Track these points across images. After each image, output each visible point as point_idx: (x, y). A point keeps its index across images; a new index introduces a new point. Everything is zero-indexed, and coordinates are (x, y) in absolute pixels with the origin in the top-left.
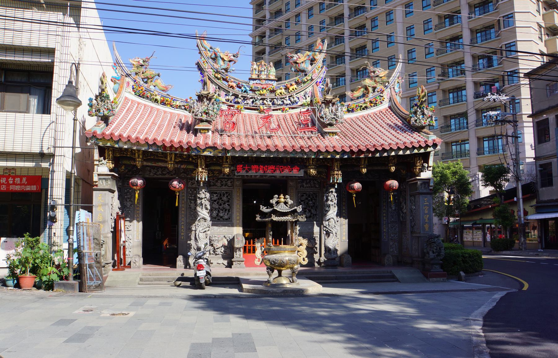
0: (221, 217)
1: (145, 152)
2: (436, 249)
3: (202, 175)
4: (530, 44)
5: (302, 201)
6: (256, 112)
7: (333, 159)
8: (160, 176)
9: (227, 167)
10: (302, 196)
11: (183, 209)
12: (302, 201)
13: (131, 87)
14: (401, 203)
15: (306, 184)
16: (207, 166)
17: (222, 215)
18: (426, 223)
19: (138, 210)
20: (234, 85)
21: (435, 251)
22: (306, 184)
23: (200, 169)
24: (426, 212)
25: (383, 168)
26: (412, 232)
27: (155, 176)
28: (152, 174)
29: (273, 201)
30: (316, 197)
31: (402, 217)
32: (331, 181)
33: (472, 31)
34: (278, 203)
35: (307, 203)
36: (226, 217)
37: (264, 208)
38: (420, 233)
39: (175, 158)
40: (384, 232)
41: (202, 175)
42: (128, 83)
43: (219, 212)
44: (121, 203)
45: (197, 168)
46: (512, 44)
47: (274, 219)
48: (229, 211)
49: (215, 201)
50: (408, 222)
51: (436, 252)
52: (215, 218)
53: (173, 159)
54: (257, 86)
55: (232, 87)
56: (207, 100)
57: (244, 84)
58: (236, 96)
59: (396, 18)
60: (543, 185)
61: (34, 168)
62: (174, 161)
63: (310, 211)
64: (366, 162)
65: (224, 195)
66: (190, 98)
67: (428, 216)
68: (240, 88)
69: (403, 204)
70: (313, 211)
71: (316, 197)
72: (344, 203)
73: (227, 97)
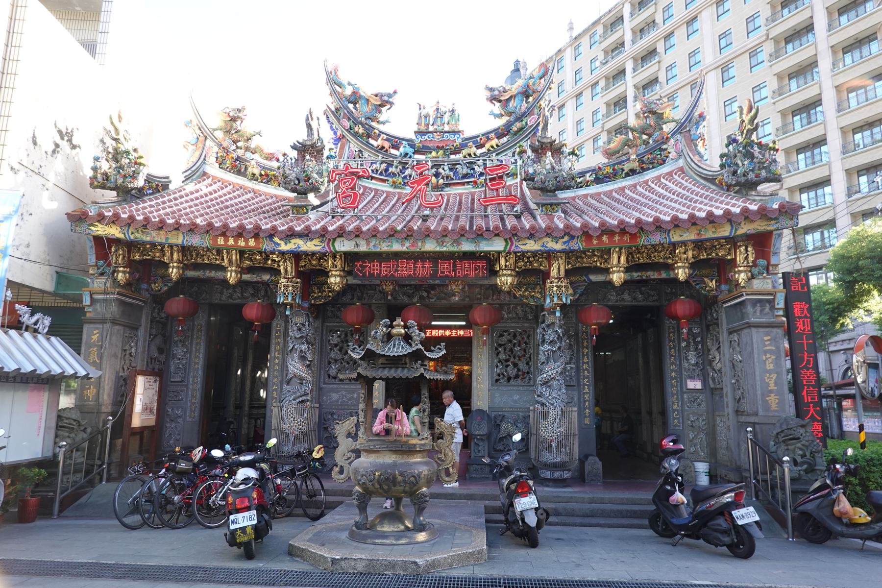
2: (803, 456)
4: (793, 586)
5: (500, 345)
9: (335, 276)
10: (501, 336)
11: (277, 361)
12: (500, 345)
15: (509, 313)
18: (771, 392)
20: (387, 145)
21: (799, 459)
22: (509, 313)
24: (770, 366)
25: (664, 275)
26: (737, 412)
28: (224, 298)
30: (528, 337)
31: (713, 379)
33: (848, 172)
34: (389, 337)
35: (511, 350)
38: (756, 414)
40: (674, 410)
49: (336, 345)
50: (727, 390)
51: (803, 463)
52: (335, 378)
59: (704, 58)
63: (515, 365)
66: (284, 155)
67: (774, 376)
69: (714, 352)
70: (522, 366)
71: (528, 337)
72: (585, 351)
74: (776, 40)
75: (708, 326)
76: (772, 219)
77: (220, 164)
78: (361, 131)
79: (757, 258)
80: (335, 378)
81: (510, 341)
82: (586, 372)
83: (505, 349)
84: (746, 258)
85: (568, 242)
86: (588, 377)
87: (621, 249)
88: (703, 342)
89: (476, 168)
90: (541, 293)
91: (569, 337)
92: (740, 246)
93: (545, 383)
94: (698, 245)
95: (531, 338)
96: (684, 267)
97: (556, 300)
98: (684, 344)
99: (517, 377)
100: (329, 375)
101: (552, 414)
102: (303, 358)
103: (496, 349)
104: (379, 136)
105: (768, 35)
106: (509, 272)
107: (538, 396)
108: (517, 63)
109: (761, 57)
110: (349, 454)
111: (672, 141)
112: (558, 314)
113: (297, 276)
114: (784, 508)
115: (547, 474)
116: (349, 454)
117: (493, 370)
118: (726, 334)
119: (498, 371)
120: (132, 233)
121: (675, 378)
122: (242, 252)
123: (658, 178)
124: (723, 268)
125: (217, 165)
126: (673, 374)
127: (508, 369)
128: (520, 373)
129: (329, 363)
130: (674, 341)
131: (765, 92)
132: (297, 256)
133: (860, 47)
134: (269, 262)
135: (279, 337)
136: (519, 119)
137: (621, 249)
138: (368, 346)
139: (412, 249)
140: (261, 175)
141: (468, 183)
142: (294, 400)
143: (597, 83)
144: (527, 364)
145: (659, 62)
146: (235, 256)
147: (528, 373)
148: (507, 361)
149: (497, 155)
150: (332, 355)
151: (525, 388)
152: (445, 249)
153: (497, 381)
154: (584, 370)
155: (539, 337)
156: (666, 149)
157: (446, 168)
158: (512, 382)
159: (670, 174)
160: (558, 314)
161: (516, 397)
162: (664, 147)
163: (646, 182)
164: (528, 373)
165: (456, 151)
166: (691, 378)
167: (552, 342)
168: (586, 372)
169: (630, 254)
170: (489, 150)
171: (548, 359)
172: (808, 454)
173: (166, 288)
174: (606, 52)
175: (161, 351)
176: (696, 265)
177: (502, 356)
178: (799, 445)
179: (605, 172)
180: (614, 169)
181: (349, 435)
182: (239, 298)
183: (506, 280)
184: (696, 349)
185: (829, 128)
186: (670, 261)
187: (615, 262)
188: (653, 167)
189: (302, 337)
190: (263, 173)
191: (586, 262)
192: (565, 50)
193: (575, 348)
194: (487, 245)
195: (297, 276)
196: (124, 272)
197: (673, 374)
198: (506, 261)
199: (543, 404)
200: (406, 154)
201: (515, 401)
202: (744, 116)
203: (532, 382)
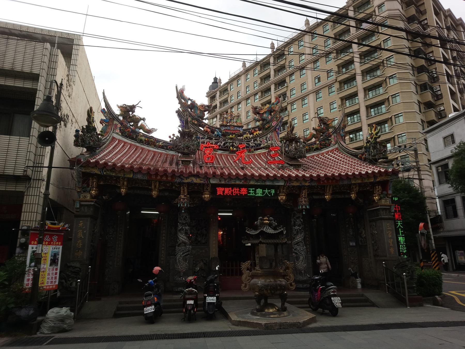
6: (227, 152)
9: (207, 194)
11: (164, 235)
13: (118, 128)
18: (391, 247)
20: (209, 130)
23: (182, 196)
24: (390, 236)
29: (258, 223)
38: (386, 256)
44: (181, 120)
45: (27, 293)
46: (400, 115)
55: (207, 131)
56: (188, 137)
59: (308, 87)
60: (448, 217)
64: (331, 191)
66: (174, 135)
67: (392, 240)
74: (340, 82)
76: (389, 175)
78: (196, 122)
79: (383, 191)
82: (307, 239)
87: (330, 186)
93: (297, 244)
97: (304, 207)
98: (347, 226)
101: (301, 258)
105: (336, 80)
106: (284, 194)
107: (295, 250)
108: (215, 79)
109: (334, 89)
110: (249, 278)
111: (333, 136)
113: (188, 194)
114: (405, 295)
116: (249, 278)
120: (105, 171)
122: (160, 182)
123: (328, 152)
126: (344, 239)
131: (335, 106)
133: (375, 89)
136: (268, 123)
137: (330, 186)
139: (245, 183)
140: (145, 140)
142: (183, 254)
143: (257, 93)
145: (287, 87)
159: (332, 150)
162: (330, 138)
163: (323, 153)
165: (241, 135)
167: (299, 226)
168: (307, 239)
171: (297, 232)
173: (111, 198)
174: (261, 79)
178: (407, 268)
181: (248, 269)
185: (363, 124)
189: (186, 223)
192: (241, 76)
194: (277, 183)
195: (188, 194)
196: (95, 190)
199: (296, 253)
200: (218, 135)
202: (373, 132)
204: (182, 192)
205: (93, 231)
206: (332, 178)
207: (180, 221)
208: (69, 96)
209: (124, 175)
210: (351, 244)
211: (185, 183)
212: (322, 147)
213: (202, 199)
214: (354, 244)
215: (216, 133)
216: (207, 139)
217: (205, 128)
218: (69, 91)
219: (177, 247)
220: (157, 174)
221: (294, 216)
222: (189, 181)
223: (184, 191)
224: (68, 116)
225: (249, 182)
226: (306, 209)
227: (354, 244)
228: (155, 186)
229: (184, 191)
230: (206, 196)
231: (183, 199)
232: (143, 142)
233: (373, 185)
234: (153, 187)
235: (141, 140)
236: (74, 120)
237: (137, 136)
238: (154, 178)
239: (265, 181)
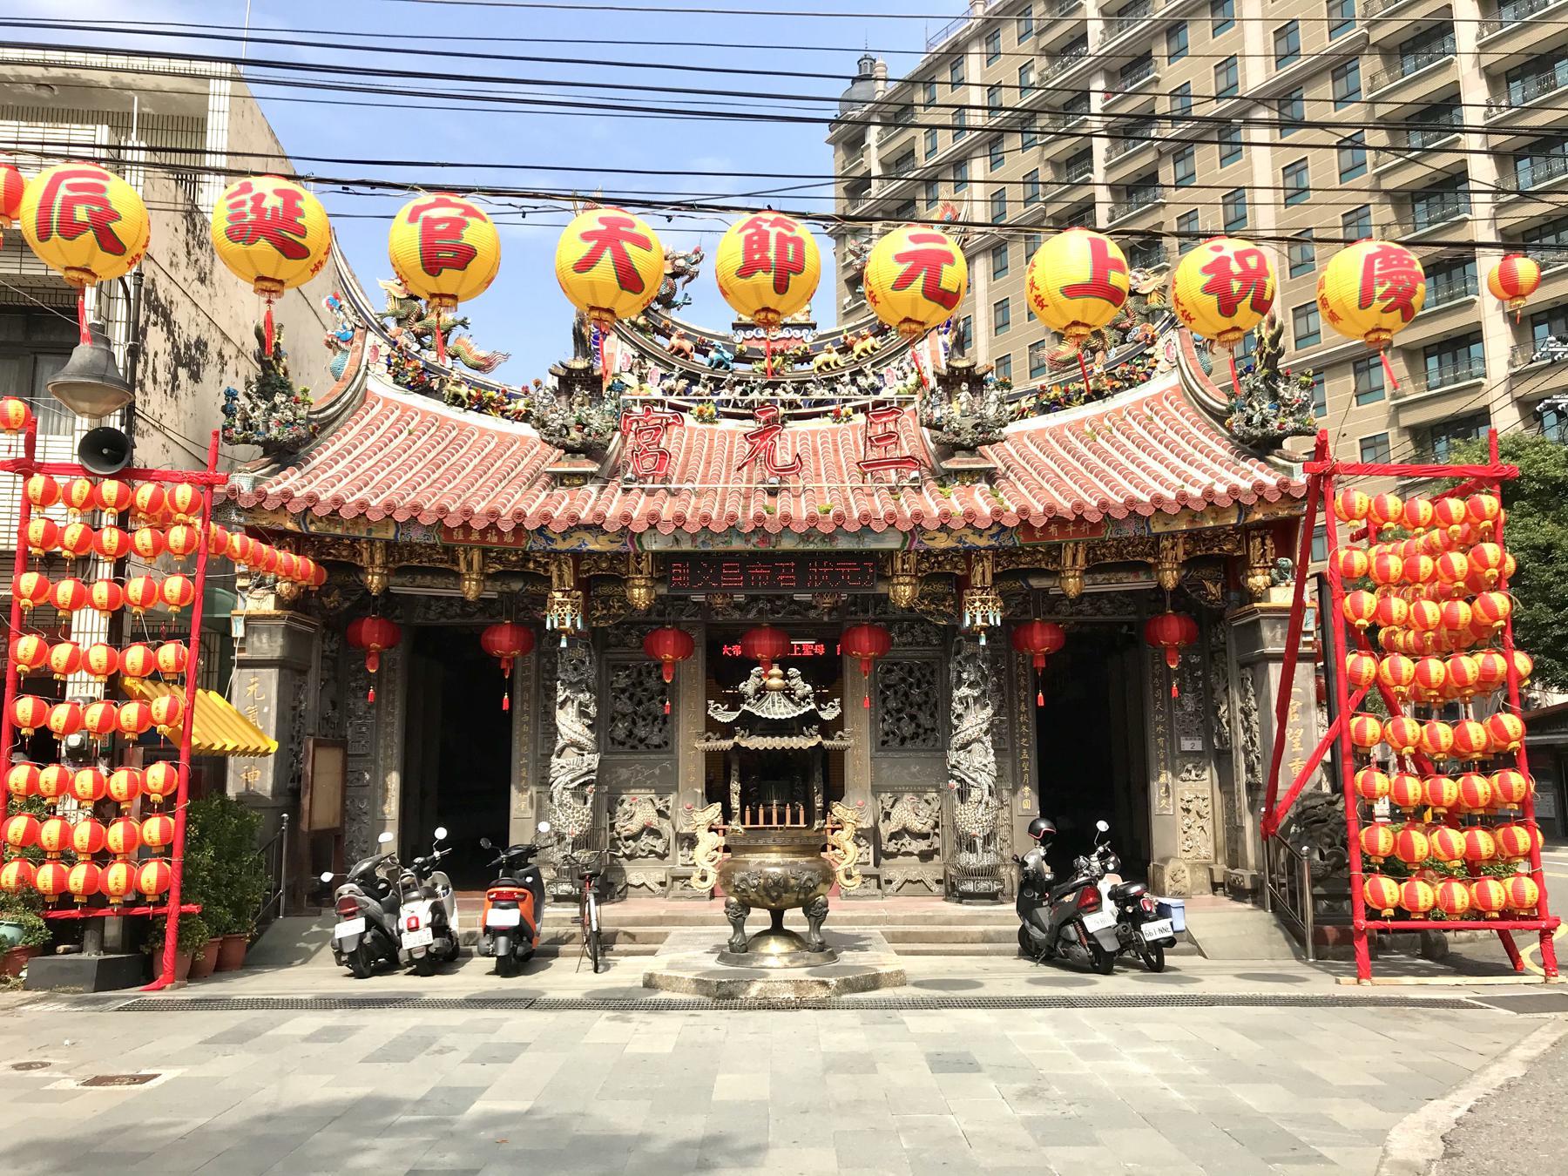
0: (641, 741)
1: (389, 546)
3: (562, 614)
5: (888, 687)
7: (969, 555)
8: (457, 620)
9: (639, 587)
10: (889, 671)
11: (526, 718)
12: (888, 687)
13: (384, 360)
14: (1213, 691)
15: (901, 634)
16: (580, 584)
17: (643, 734)
19: (387, 725)
20: (687, 345)
22: (901, 634)
23: (558, 596)
27: (443, 620)
28: (431, 615)
29: (748, 687)
32: (968, 622)
34: (762, 692)
35: (906, 694)
36: (656, 740)
37: (721, 709)
39: (484, 565)
41: (562, 614)
42: (375, 349)
43: (634, 723)
47: (743, 744)
48: (665, 722)
49: (623, 691)
52: (623, 744)
53: (476, 566)
54: (754, 345)
55: (680, 351)
57: (716, 342)
58: (693, 379)
61: (1003, 697)
62: (481, 572)
63: (913, 718)
65: (649, 673)
66: (537, 384)
68: (706, 354)
70: (924, 719)
71: (932, 673)
72: (1023, 694)
73: (668, 383)
75: (1212, 653)
77: (395, 377)
80: (623, 744)
81: (903, 680)
83: (896, 693)
84: (1263, 555)
85: (998, 534)
86: (1027, 735)
87: (1076, 544)
88: (1205, 678)
89: (839, 387)
90: (954, 606)
91: (998, 673)
92: (1254, 537)
94: (1194, 536)
95: (937, 675)
96: (1172, 570)
99: (915, 736)
100: (613, 739)
102: (583, 714)
103: (882, 692)
104: (673, 329)
106: (907, 579)
112: (983, 642)
115: (969, 887)
117: (877, 725)
118: (1235, 666)
119: (886, 728)
121: (1163, 735)
122: (485, 552)
124: (1233, 570)
125: (390, 378)
127: (902, 724)
128: (921, 731)
129: (613, 719)
130: (1160, 677)
132: (578, 556)
134: (531, 565)
135: (527, 678)
137: (1076, 544)
138: (745, 707)
141: (825, 414)
144: (932, 715)
146: (476, 556)
147: (933, 730)
148: (899, 711)
149: (873, 365)
150: (619, 706)
151: (928, 755)
152: (811, 547)
153: (884, 743)
154: (1021, 724)
155: (953, 675)
156: (1151, 356)
157: (789, 389)
158: (908, 745)
160: (983, 642)
161: (914, 769)
164: (933, 730)
165: (806, 358)
166: (1187, 734)
167: (971, 685)
169: (1090, 549)
170: (859, 356)
172: (1338, 842)
173: (347, 605)
175: (334, 705)
176: (1190, 563)
177: (892, 704)
178: (1326, 830)
179: (1052, 395)
180: (1067, 391)
182: (457, 615)
183: (904, 592)
184: (1195, 690)
186: (1151, 560)
187: (1069, 563)
188: (1131, 386)
189: (580, 681)
190: (473, 393)
191: (1025, 563)
193: (1006, 689)
197: (1160, 728)
198: (904, 562)
200: (720, 364)
201: (914, 775)
203: (939, 745)
204: (555, 580)
205: (294, 708)
206: (1073, 517)
207: (562, 676)
208: (202, 281)
209: (370, 531)
210: (1187, 745)
211: (561, 552)
212: (1118, 384)
213: (627, 604)
214: (1198, 746)
215: (713, 354)
216: (681, 377)
217: (674, 340)
218: (201, 262)
219: (554, 758)
220: (466, 527)
221: (958, 653)
222: (571, 544)
223: (560, 577)
224: (201, 345)
225: (778, 542)
226: (990, 631)
227: (1198, 746)
228: (470, 564)
229: (560, 577)
230: (636, 591)
231: (561, 604)
232: (462, 405)
233: (1246, 531)
234: (463, 567)
235: (457, 396)
236: (229, 351)
237: (442, 383)
238: (461, 537)
239: (471, 615)
